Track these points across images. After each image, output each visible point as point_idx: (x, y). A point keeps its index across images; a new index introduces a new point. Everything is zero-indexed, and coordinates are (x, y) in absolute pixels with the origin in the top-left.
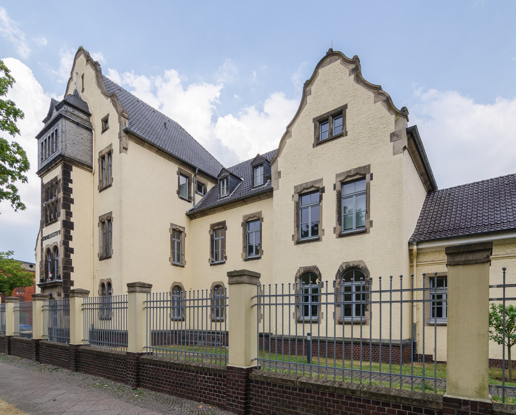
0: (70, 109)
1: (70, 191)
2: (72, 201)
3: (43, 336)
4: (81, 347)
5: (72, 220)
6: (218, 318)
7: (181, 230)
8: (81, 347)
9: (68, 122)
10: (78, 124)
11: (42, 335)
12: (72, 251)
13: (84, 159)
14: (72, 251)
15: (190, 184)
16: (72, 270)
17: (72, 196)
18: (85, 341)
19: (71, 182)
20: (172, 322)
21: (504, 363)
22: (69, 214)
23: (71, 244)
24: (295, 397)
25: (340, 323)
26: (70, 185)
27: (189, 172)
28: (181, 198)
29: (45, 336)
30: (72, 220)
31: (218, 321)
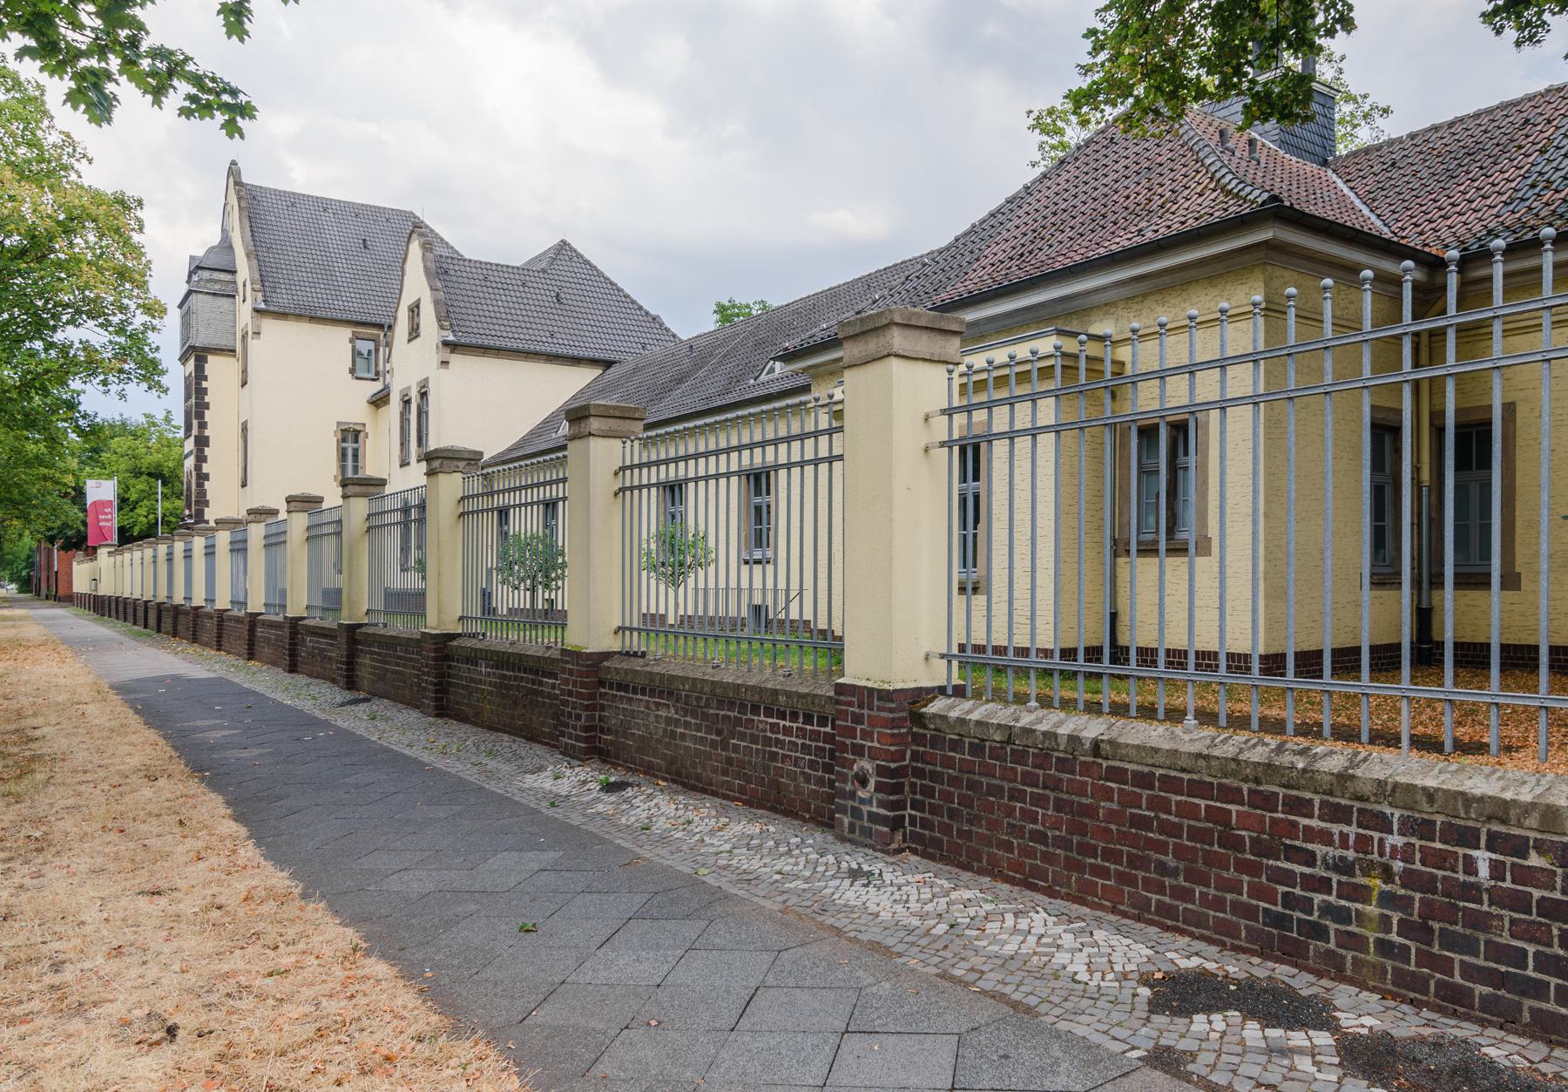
0: (206, 274)
1: (205, 391)
2: (207, 406)
3: (461, 618)
4: (364, 630)
5: (207, 433)
6: (758, 555)
7: (358, 428)
8: (364, 630)
9: (200, 296)
10: (214, 294)
11: (460, 614)
12: (206, 477)
13: (223, 342)
14: (206, 477)
15: (377, 350)
16: (207, 504)
17: (207, 399)
18: (627, 633)
19: (206, 378)
20: (745, 569)
21: (787, 625)
22: (203, 426)
23: (206, 468)
24: (1282, 816)
25: (746, 562)
26: (204, 384)
27: (375, 332)
28: (357, 378)
29: (467, 618)
30: (207, 433)
31: (758, 562)
